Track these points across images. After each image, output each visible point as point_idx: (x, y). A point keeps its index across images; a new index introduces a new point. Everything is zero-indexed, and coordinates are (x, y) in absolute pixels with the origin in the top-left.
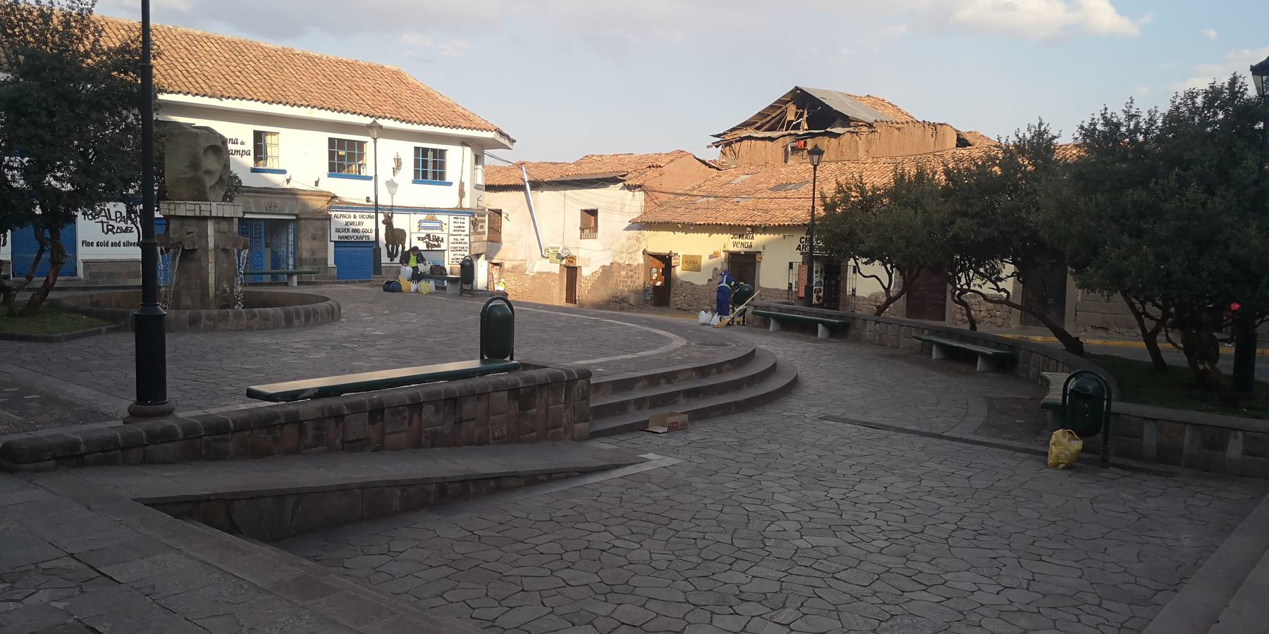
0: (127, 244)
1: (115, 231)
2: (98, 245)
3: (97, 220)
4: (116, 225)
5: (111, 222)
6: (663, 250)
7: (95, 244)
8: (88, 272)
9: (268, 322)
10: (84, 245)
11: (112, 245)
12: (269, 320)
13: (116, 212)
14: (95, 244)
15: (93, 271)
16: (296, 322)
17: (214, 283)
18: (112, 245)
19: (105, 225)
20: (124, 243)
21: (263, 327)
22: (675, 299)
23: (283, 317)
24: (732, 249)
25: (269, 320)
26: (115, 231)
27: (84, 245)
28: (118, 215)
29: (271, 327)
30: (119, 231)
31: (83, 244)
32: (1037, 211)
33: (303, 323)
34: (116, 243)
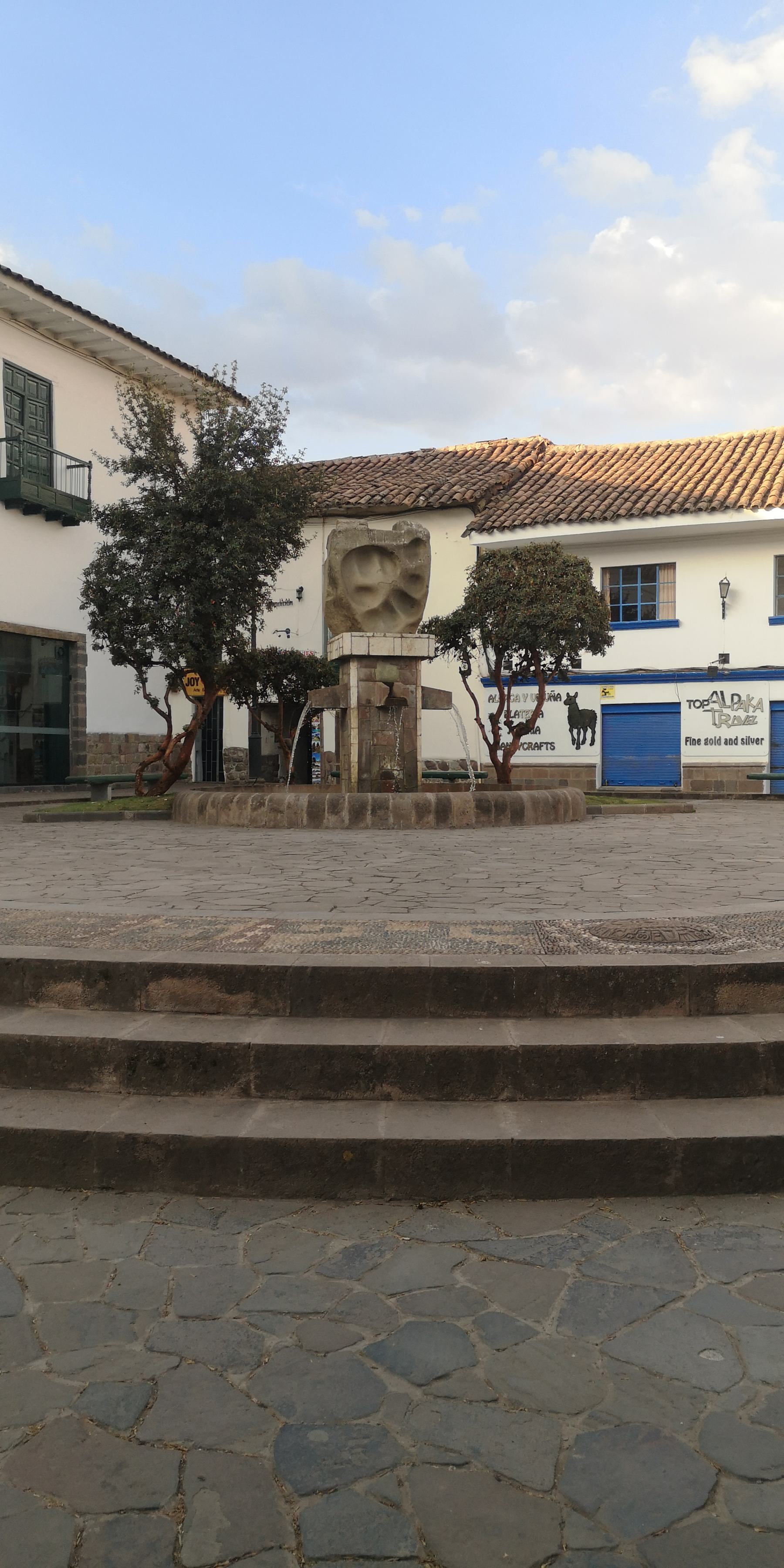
0: (748, 741)
1: (730, 722)
2: (706, 744)
3: (706, 708)
4: (732, 714)
5: (726, 711)
6: (768, 704)
7: (703, 742)
8: (690, 780)
9: (279, 815)
10: (688, 743)
11: (726, 743)
12: (281, 812)
13: (733, 695)
14: (703, 742)
15: (695, 778)
16: (330, 819)
17: (357, 760)
18: (726, 743)
19: (717, 714)
20: (742, 739)
21: (272, 823)
22: (514, 778)
23: (305, 809)
24: (106, 655)
25: (281, 812)
26: (730, 722)
27: (688, 743)
28: (736, 699)
29: (285, 823)
30: (736, 722)
31: (687, 741)
32: (137, 558)
33: (347, 822)
34: (731, 739)
